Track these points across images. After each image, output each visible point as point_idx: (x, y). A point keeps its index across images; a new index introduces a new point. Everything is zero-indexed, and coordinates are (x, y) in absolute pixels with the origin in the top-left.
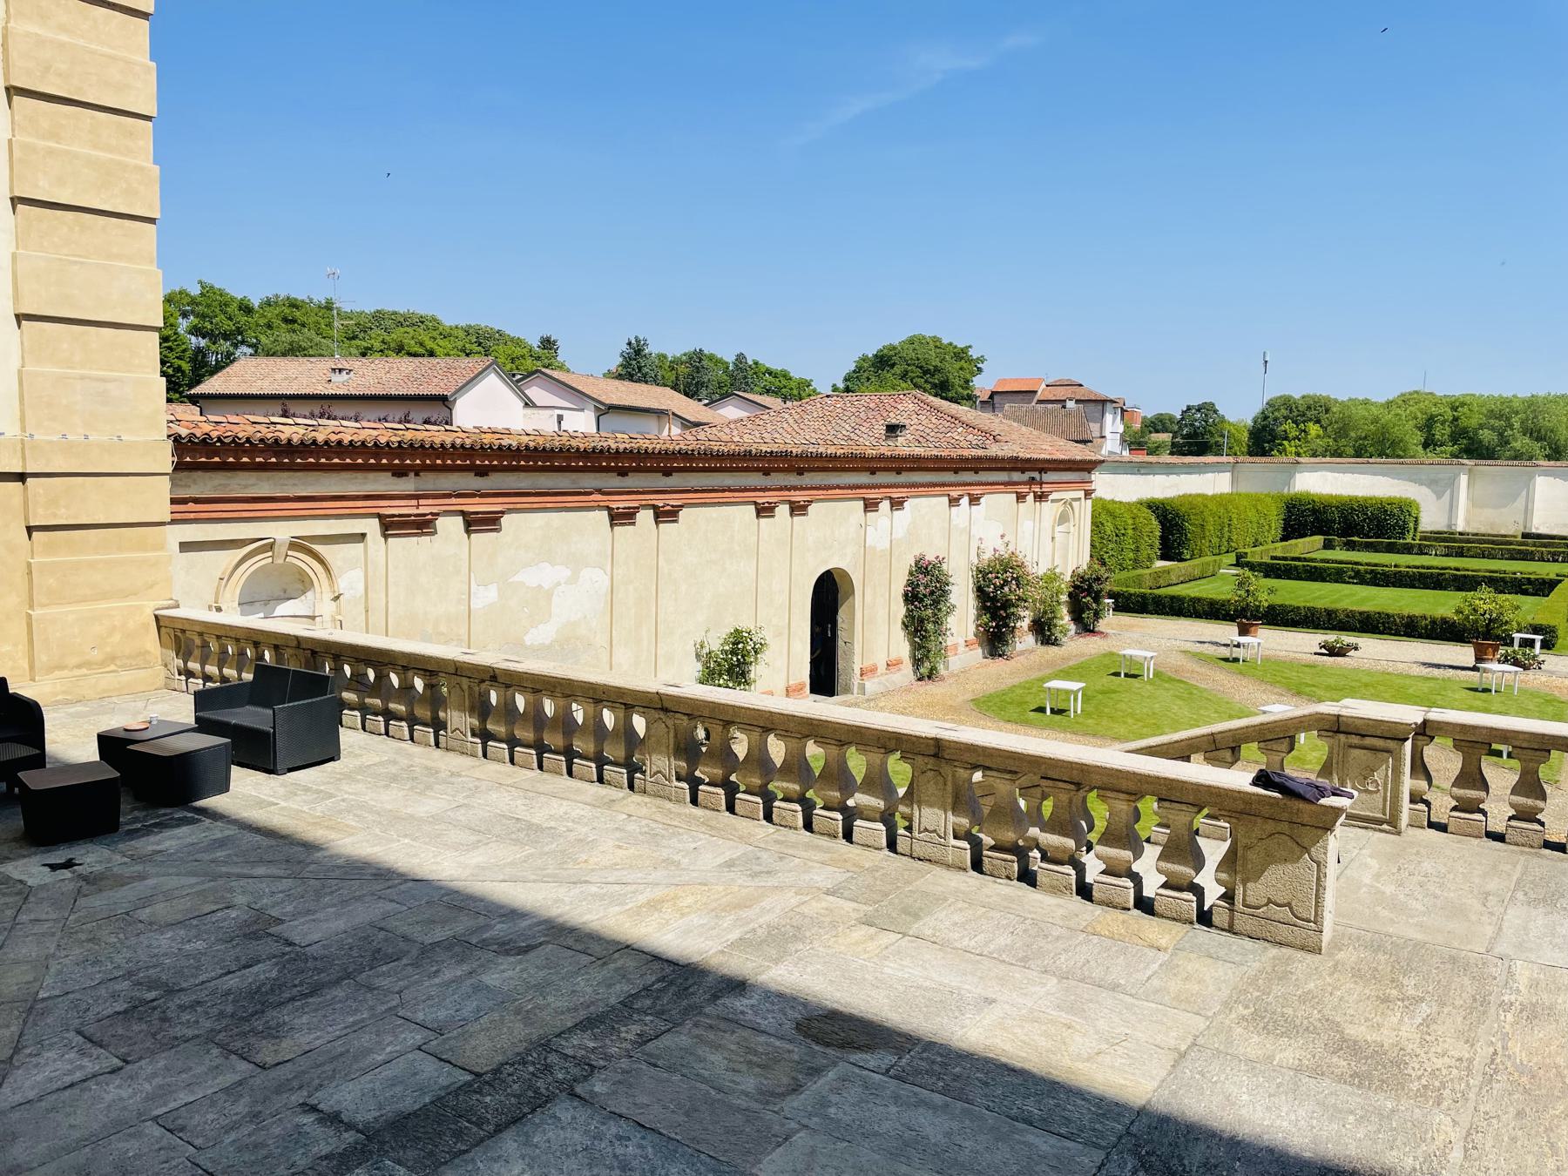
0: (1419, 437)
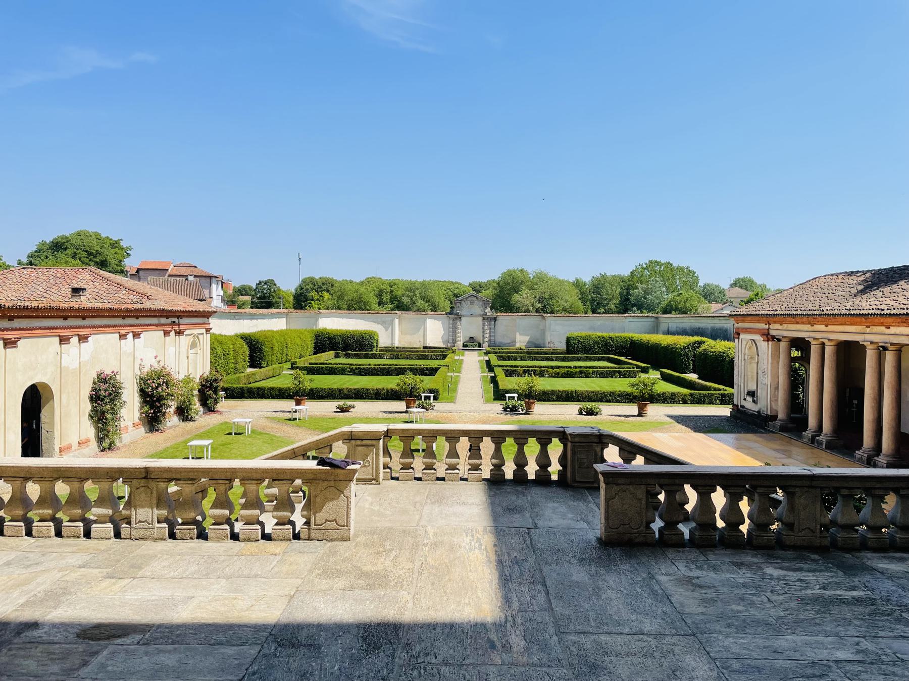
0: (377, 300)
